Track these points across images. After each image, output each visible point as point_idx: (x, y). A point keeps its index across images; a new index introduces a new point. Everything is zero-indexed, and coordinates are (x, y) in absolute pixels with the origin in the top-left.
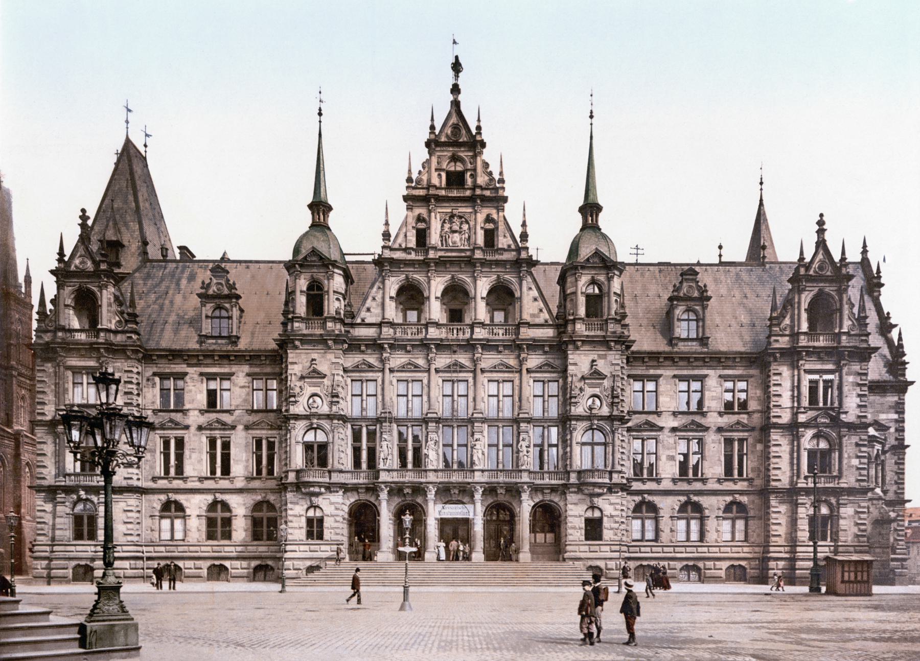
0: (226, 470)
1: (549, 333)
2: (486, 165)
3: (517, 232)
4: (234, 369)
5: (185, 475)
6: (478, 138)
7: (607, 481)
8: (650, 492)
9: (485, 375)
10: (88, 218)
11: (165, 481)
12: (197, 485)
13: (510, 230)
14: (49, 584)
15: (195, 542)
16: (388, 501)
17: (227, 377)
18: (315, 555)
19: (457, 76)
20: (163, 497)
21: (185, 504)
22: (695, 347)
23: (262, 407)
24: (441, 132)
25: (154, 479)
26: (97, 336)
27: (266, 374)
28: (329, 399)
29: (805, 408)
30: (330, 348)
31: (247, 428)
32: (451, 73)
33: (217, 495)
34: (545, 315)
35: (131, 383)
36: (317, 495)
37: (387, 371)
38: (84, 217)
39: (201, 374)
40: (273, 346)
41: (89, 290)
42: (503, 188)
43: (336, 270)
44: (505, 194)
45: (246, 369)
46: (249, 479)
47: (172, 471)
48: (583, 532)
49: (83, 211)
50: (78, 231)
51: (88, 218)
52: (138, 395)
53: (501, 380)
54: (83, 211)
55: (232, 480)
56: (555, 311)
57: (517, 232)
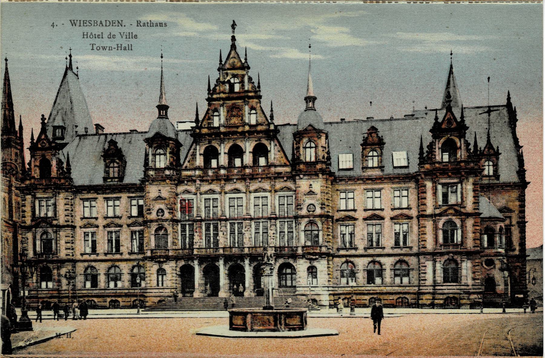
0: (118, 250)
1: (288, 169)
2: (250, 79)
3: (268, 114)
4: (356, 187)
5: (97, 252)
6: (246, 65)
7: (318, 251)
8: (350, 256)
9: (227, 195)
10: (46, 119)
11: (111, 255)
12: (104, 257)
13: (264, 113)
14: (433, 308)
15: (103, 288)
16: (250, 265)
17: (118, 199)
18: (162, 294)
19: (233, 32)
20: (86, 264)
21: (97, 267)
22: (377, 173)
23: (345, 208)
24: (226, 62)
25: (338, 249)
26: (50, 181)
27: (137, 197)
28: (320, 206)
29: (440, 205)
30: (301, 179)
31: (129, 226)
32: (230, 29)
33: (348, 258)
34: (284, 160)
35: (68, 204)
36: (163, 262)
37: (198, 194)
38: (43, 119)
39: (104, 198)
40: (138, 182)
41: (452, 139)
42: (260, 91)
43: (171, 142)
44: (261, 94)
45: (390, 185)
46: (365, 249)
47: (114, 250)
48: (366, 280)
49: (43, 116)
50: (40, 126)
51: (46, 119)
52: (72, 211)
53: (211, 198)
54: (43, 116)
55: (122, 254)
56: (290, 157)
57: (268, 114)
